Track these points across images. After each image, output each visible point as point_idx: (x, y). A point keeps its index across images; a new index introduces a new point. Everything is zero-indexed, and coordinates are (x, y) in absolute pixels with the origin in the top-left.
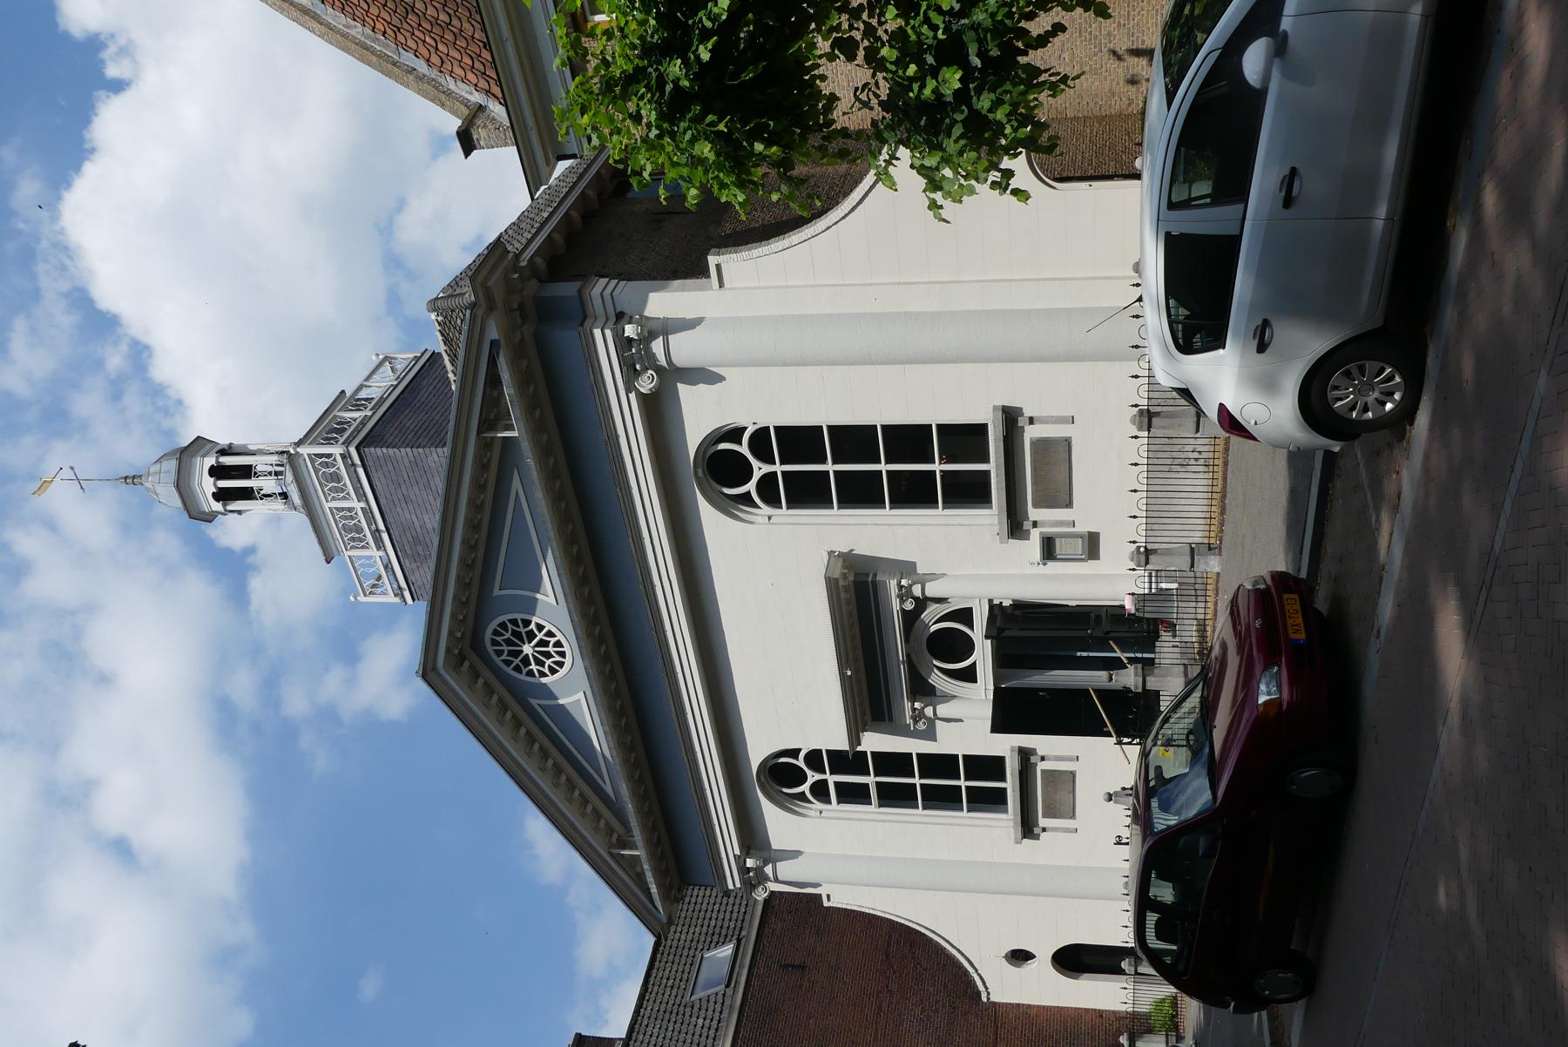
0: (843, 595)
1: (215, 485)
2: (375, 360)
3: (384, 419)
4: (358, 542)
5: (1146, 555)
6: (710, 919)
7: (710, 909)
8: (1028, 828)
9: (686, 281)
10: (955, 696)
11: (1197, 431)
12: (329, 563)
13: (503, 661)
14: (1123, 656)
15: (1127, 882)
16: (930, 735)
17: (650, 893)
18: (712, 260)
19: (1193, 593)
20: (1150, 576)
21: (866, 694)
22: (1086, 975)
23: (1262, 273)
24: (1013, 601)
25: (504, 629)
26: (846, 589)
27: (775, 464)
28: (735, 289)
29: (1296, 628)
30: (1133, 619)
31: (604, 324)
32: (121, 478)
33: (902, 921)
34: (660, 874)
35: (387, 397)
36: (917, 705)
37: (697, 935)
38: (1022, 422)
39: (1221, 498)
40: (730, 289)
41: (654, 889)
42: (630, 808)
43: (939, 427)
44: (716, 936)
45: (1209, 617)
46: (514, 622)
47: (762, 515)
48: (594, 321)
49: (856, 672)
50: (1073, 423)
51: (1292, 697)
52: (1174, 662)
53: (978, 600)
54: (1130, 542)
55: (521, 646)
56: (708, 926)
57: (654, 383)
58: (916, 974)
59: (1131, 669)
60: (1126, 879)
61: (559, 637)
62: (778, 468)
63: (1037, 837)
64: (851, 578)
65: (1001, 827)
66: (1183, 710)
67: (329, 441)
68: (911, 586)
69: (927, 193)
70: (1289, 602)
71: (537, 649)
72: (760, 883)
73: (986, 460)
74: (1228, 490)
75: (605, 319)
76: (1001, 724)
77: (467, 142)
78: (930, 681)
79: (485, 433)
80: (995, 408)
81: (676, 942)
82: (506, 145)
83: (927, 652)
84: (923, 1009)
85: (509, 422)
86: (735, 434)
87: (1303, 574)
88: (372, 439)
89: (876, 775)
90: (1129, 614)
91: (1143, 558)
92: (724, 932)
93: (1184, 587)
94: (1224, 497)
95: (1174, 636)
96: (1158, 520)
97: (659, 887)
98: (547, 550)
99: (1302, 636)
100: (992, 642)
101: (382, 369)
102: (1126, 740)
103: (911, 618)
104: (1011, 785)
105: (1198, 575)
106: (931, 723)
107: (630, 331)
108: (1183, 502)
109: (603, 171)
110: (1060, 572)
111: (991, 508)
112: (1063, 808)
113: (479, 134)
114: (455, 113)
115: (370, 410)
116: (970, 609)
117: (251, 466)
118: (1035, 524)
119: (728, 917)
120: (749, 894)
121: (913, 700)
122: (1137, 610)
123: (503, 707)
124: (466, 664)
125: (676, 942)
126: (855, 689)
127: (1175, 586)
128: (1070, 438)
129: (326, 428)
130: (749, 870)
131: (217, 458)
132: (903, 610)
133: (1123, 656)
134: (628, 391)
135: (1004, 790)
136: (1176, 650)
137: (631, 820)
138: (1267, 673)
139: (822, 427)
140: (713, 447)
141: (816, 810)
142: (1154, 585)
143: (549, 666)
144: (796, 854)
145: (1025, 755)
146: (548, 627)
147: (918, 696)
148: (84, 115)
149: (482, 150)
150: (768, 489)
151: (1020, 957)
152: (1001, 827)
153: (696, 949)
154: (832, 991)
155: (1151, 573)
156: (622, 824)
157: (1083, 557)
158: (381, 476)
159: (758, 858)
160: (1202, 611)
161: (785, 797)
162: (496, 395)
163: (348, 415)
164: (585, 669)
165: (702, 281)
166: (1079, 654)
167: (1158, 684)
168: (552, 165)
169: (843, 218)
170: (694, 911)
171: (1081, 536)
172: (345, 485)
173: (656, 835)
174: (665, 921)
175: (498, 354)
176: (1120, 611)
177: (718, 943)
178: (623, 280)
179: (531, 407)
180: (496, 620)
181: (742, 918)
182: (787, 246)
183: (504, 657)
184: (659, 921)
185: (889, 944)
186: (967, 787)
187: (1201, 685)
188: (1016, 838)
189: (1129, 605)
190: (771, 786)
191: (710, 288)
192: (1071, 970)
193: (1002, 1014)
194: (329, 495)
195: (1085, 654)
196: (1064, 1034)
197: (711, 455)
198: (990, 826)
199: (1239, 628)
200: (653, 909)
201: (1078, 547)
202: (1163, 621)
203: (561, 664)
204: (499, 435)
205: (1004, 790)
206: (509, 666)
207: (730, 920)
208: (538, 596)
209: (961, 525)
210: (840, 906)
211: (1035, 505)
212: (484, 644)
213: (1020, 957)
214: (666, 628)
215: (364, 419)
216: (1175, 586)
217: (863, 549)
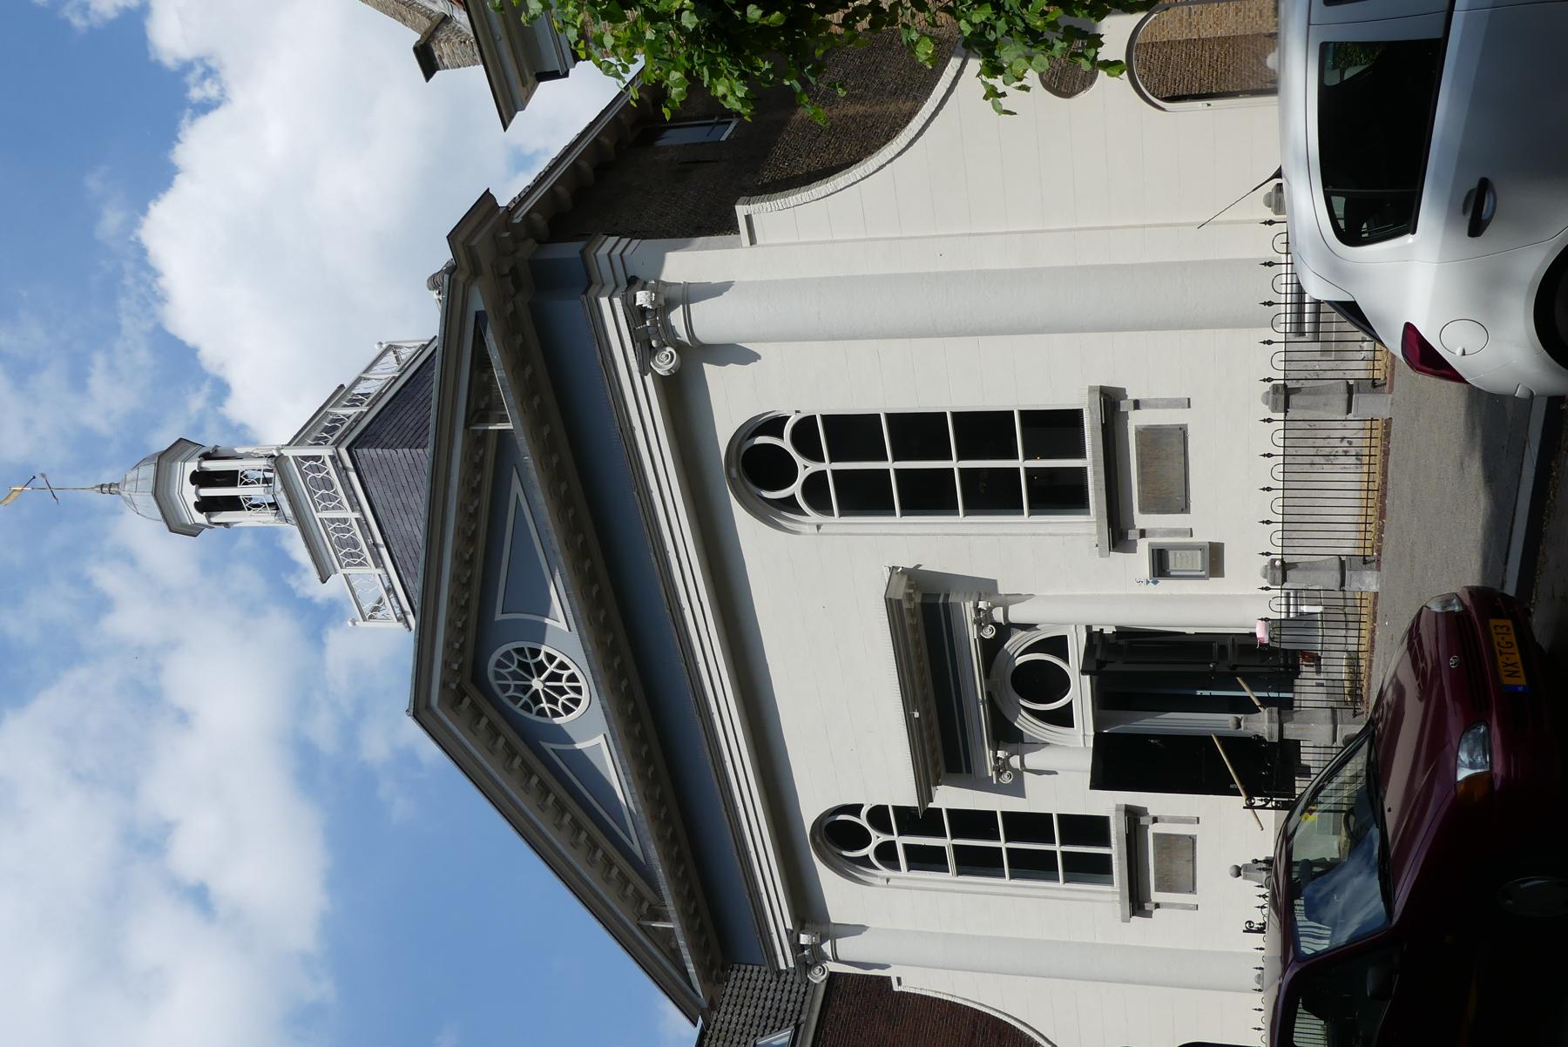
0: (908, 621)
1: (197, 493)
2: (378, 350)
3: (381, 416)
4: (354, 558)
5: (1282, 570)
6: (766, 999)
7: (766, 987)
8: (1138, 903)
9: (712, 237)
10: (1048, 744)
11: (1349, 411)
12: (324, 582)
13: (510, 697)
14: (1254, 696)
15: (1259, 975)
16: (1017, 789)
17: (687, 973)
18: (741, 210)
19: (1342, 618)
20: (1288, 597)
21: (938, 742)
23: (1480, 97)
24: (1116, 627)
25: (508, 660)
26: (912, 613)
28: (770, 245)
29: (1512, 671)
30: (1266, 651)
31: (614, 291)
32: (97, 487)
33: (987, 1011)
34: (699, 951)
35: (385, 393)
36: (1000, 754)
37: (767, 1009)
38: (1125, 406)
39: (1379, 497)
40: (763, 246)
41: (691, 969)
42: (660, 872)
43: (1023, 413)
44: (771, 1021)
45: (1362, 648)
46: (520, 651)
47: (809, 524)
48: (601, 288)
49: (925, 713)
50: (1189, 407)
51: (1508, 772)
52: (1319, 704)
53: (1073, 627)
54: (1263, 554)
55: (529, 680)
56: (763, 1008)
57: (673, 363)
59: (1264, 713)
60: (1259, 972)
61: (573, 669)
62: (828, 466)
63: (1148, 914)
64: (918, 600)
65: (1104, 902)
66: (1340, 780)
67: (318, 442)
68: (990, 609)
69: (984, 77)
70: (1499, 630)
71: (548, 684)
72: (816, 963)
74: (1389, 486)
75: (614, 286)
76: (1103, 778)
77: (428, 62)
78: (1016, 724)
79: (474, 425)
80: (1091, 389)
81: (726, 1024)
82: (475, 63)
85: (504, 413)
86: (774, 425)
87: (1511, 589)
88: (367, 437)
90: (1261, 645)
91: (1279, 574)
92: (780, 1016)
93: (1329, 611)
94: (1383, 496)
95: (1318, 672)
96: (1297, 526)
97: (698, 965)
98: (555, 569)
99: (1521, 681)
100: (1091, 678)
101: (384, 360)
102: (1258, 801)
103: (992, 649)
104: (1116, 850)
105: (1348, 595)
106: (1018, 775)
107: (642, 298)
108: (1328, 502)
109: (622, 116)
110: (1175, 592)
111: (1089, 514)
112: (1181, 877)
113: (442, 49)
114: (415, 28)
115: (367, 405)
116: (1065, 637)
117: (237, 471)
118: (1143, 533)
120: (803, 974)
121: (995, 750)
122: (1271, 639)
123: (511, 752)
124: (467, 701)
125: (726, 1024)
126: (925, 734)
127: (1319, 609)
128: (1186, 425)
129: (319, 428)
130: (803, 947)
131: (200, 462)
132: (982, 639)
133: (1254, 696)
134: (643, 373)
135: (1108, 857)
136: (1321, 689)
137: (662, 887)
138: (1470, 736)
139: (879, 415)
140: (749, 441)
141: (882, 878)
142: (1292, 609)
144: (858, 929)
145: (1133, 816)
146: (560, 658)
147: (1001, 742)
148: (170, 136)
149: (446, 71)
150: (816, 490)
152: (1104, 902)
153: (748, 1035)
155: (1288, 594)
157: (1203, 573)
159: (813, 933)
160: (1355, 641)
161: (843, 859)
162: (486, 379)
163: (341, 412)
164: (603, 708)
165: (731, 238)
166: (1199, 693)
167: (1300, 732)
168: (529, 86)
169: (899, 154)
170: (747, 989)
171: (1200, 548)
173: (693, 905)
175: (485, 328)
176: (1250, 641)
177: (773, 1028)
178: (625, 237)
179: (528, 392)
180: (498, 650)
181: (801, 1000)
182: (831, 191)
183: (510, 693)
184: (698, 1006)
186: (1063, 853)
187: (1366, 745)
188: (1123, 916)
189: (1262, 634)
190: (826, 847)
191: (739, 245)
195: (1206, 693)
197: (748, 449)
198: (1091, 901)
199: (1422, 665)
200: (690, 991)
201: (1197, 561)
202: (1303, 653)
203: (577, 702)
204: (490, 428)
205: (1108, 857)
206: (516, 703)
207: (788, 1001)
208: (547, 621)
209: (1050, 535)
210: (912, 991)
211: (1143, 510)
212: (487, 675)
215: (358, 417)
216: (1319, 609)
217: (932, 564)
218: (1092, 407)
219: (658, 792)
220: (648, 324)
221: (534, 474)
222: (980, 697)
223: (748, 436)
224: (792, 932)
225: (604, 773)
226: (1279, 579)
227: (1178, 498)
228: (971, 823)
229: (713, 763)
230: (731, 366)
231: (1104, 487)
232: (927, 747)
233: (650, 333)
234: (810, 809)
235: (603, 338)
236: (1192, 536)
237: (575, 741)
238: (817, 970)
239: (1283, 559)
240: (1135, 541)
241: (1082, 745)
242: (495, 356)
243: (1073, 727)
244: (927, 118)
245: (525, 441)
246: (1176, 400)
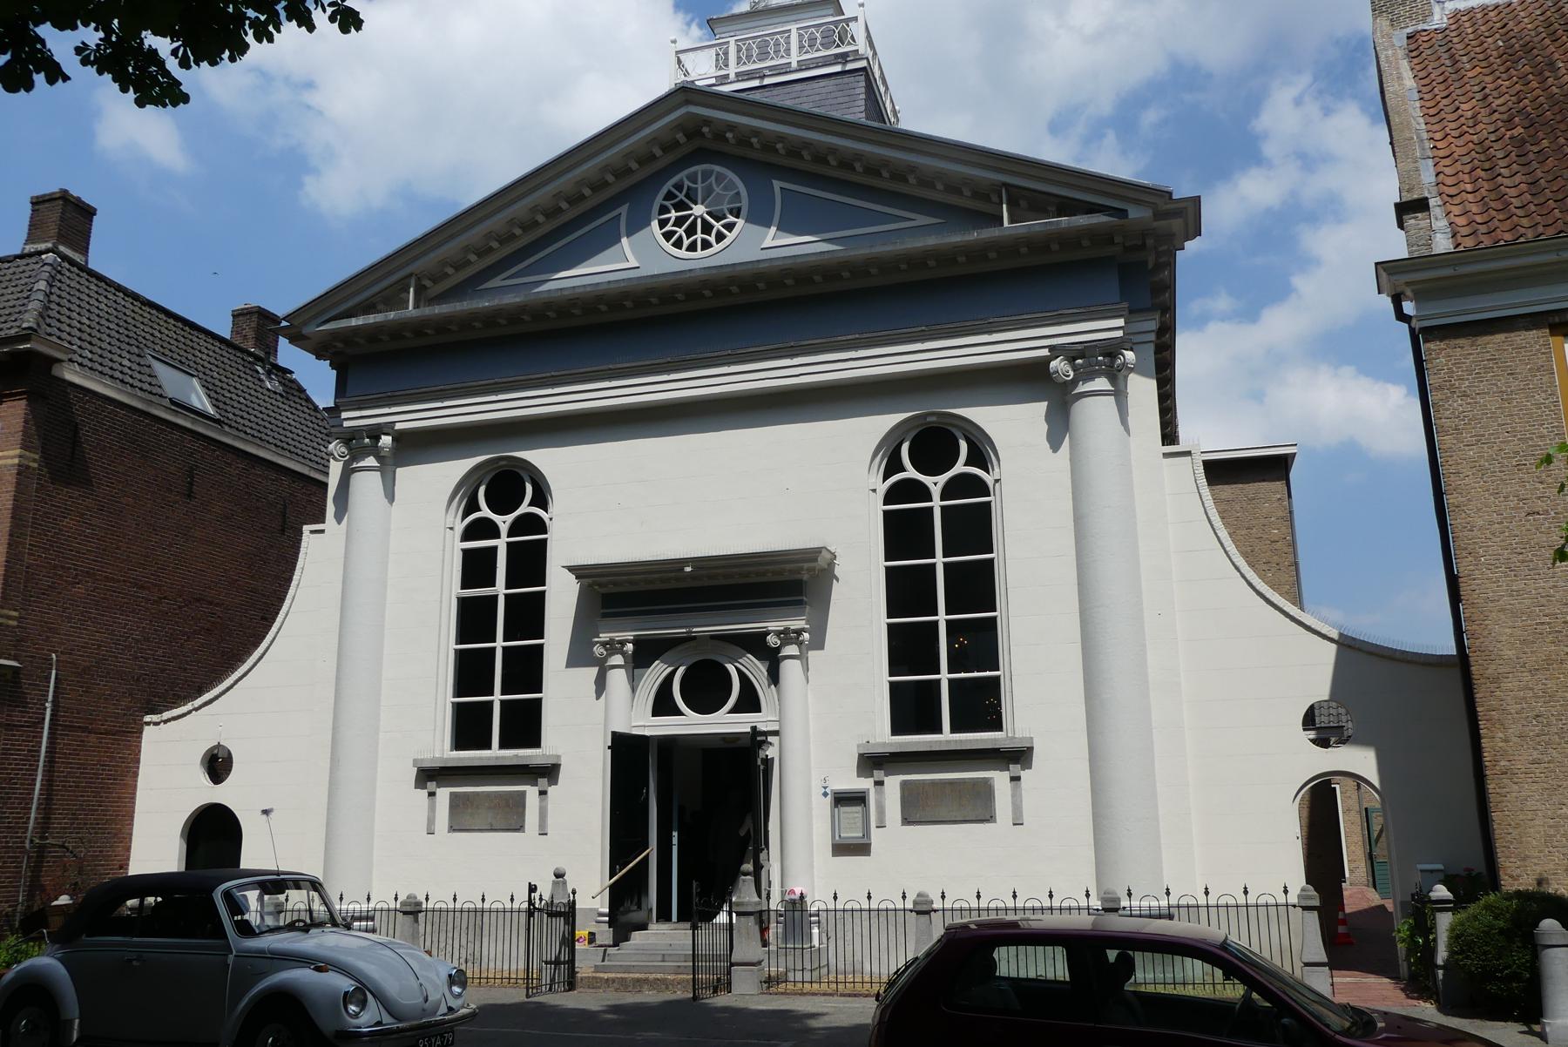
8: (430, 776)
10: (634, 690)
11: (1307, 964)
22: (185, 846)
27: (508, 537)
34: (373, 333)
36: (630, 647)
38: (1015, 769)
41: (354, 322)
47: (454, 522)
50: (1014, 824)
58: (177, 635)
64: (805, 577)
71: (699, 221)
73: (502, 746)
78: (657, 662)
83: (694, 661)
84: (137, 641)
86: (541, 499)
89: (506, 596)
91: (408, 909)
97: (357, 329)
103: (755, 644)
111: (451, 750)
118: (879, 783)
119: (237, 412)
120: (338, 436)
128: (995, 822)
132: (768, 633)
134: (1051, 348)
143: (676, 232)
144: (390, 496)
146: (730, 236)
151: (218, 765)
154: (163, 528)
156: (436, 297)
157: (837, 838)
158: (831, 88)
166: (675, 834)
172: (818, 50)
174: (304, 332)
175: (1108, 215)
180: (737, 178)
184: (305, 323)
185: (211, 603)
192: (190, 829)
193: (129, 741)
194: (744, 44)
195: (675, 841)
196: (103, 819)
197: (518, 474)
201: (852, 834)
203: (678, 244)
208: (773, 229)
211: (904, 784)
213: (218, 765)
214: (732, 367)
217: (840, 594)
219: (429, 331)
220: (1099, 358)
221: (931, 241)
222: (694, 630)
223: (969, 436)
224: (393, 428)
225: (601, 256)
226: (405, 909)
227: (918, 815)
228: (528, 615)
229: (610, 369)
230: (1046, 427)
231: (933, 749)
232: (656, 576)
233: (1091, 359)
234: (543, 458)
235: (1084, 317)
236: (877, 827)
237: (747, 224)
238: (343, 449)
240: (426, 788)
241: (634, 724)
242: (1082, 220)
243: (653, 716)
244: (1285, 609)
245: (993, 235)
246: (1021, 812)
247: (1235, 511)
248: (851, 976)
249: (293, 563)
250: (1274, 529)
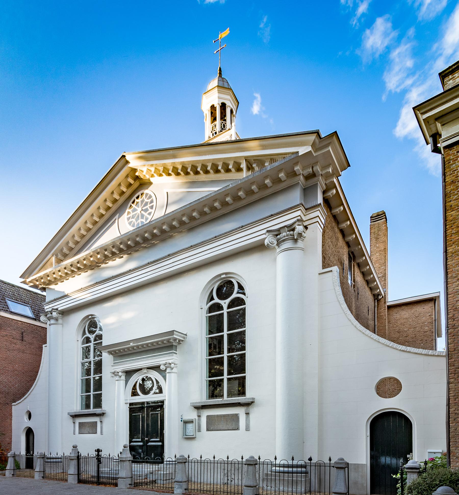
8: (75, 416)
11: (246, 486)
19: (168, 478)
54: (109, 454)
80: (253, 399)
104: (92, 410)
128: (239, 430)
132: (160, 365)
197: (231, 281)
218: (246, 399)
239: (187, 462)
247: (409, 322)
248: (160, 485)
249: (222, 319)
250: (426, 327)
